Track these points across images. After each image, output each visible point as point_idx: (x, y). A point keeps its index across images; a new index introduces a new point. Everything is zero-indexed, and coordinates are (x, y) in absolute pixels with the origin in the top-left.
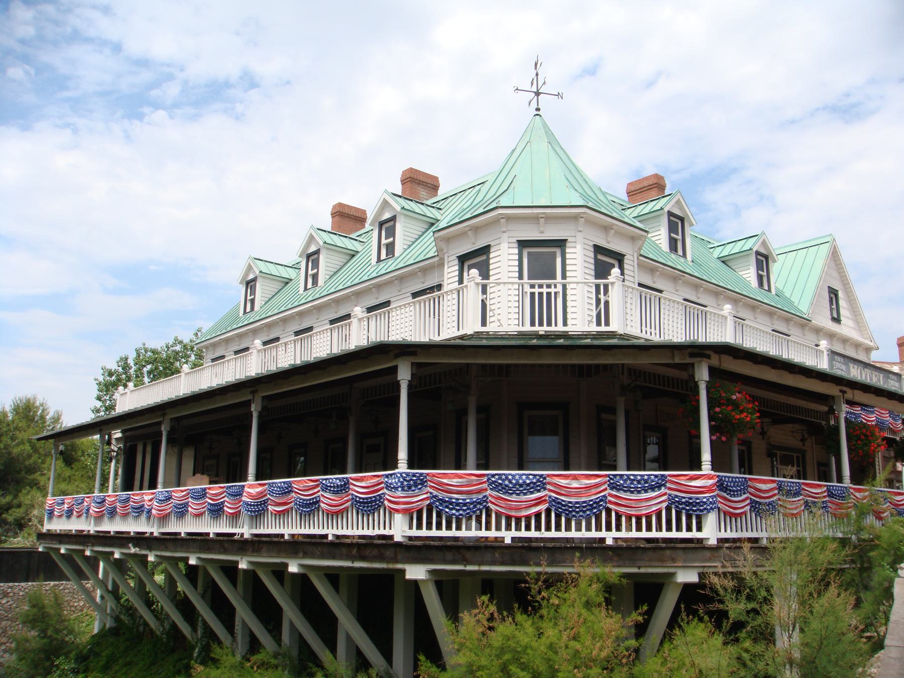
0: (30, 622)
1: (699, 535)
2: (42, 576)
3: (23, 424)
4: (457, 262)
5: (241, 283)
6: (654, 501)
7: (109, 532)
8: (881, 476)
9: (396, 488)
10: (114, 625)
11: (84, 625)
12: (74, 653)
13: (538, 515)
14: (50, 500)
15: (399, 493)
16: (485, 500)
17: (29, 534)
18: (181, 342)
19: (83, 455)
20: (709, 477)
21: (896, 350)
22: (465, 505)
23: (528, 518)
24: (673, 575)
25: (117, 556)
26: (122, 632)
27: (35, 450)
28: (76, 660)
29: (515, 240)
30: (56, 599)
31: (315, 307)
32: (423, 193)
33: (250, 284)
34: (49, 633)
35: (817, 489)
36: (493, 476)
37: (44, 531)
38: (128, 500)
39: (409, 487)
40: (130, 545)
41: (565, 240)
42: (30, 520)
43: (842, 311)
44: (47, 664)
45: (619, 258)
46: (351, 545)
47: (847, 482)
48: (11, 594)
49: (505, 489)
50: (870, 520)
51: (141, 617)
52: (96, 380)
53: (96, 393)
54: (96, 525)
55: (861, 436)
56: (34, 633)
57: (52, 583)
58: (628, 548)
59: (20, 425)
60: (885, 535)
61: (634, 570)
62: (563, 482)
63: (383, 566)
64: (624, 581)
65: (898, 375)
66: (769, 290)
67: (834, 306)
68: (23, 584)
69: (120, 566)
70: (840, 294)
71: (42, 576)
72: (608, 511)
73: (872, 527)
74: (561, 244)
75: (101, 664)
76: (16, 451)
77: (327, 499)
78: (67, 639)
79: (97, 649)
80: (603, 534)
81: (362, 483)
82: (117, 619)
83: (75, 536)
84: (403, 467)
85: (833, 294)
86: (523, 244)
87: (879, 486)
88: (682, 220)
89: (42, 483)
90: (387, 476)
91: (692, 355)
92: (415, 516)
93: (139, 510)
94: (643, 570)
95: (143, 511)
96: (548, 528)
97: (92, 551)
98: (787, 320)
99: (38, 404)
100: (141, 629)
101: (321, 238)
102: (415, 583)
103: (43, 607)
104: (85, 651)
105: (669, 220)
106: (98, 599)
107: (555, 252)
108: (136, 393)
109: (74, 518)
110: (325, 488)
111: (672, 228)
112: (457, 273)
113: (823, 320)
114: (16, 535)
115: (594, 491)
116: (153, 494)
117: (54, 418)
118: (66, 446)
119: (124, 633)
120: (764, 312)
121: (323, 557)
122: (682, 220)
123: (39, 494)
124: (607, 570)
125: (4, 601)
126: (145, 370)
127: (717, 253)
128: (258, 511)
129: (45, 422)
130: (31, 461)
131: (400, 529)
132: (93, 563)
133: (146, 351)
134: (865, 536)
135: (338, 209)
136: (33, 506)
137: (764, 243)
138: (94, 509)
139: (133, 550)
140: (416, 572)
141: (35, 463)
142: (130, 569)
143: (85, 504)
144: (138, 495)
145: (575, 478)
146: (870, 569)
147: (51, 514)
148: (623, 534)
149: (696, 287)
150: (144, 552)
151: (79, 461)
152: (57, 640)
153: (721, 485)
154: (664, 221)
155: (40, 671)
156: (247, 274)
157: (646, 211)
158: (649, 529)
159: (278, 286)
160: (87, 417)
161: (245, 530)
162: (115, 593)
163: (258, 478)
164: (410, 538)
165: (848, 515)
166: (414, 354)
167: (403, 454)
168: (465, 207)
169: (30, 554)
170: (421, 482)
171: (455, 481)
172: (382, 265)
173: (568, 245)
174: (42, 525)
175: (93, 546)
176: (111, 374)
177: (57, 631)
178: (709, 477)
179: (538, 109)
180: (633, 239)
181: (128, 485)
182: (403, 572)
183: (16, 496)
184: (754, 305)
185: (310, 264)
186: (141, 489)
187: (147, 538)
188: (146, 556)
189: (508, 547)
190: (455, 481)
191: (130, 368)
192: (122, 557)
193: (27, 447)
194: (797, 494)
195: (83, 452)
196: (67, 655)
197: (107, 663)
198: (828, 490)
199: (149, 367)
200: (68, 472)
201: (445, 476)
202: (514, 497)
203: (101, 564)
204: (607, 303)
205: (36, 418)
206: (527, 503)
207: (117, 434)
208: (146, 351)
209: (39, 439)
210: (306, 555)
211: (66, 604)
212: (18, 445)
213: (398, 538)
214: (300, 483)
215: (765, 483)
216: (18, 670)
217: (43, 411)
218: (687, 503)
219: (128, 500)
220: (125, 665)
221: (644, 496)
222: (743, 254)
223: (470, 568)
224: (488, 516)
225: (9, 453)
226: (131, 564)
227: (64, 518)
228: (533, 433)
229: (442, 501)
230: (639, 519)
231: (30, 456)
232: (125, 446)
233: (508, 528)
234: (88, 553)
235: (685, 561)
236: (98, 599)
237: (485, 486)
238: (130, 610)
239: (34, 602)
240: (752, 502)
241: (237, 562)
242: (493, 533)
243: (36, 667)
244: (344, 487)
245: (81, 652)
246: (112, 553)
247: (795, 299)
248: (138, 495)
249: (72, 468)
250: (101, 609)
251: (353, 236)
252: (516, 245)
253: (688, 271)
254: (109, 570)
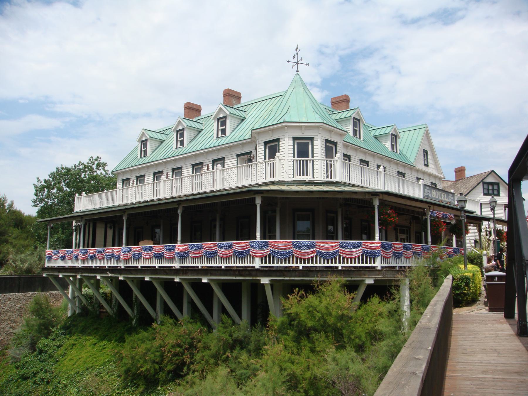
1: (374, 265)
2: (40, 289)
4: (263, 144)
5: (138, 142)
6: (357, 252)
8: (444, 242)
9: (256, 247)
10: (80, 311)
13: (312, 258)
15: (258, 249)
16: (292, 252)
18: (83, 164)
20: (378, 243)
21: (454, 174)
22: (284, 254)
23: (308, 259)
24: (364, 280)
29: (291, 136)
31: (183, 158)
32: (234, 101)
33: (144, 143)
35: (418, 247)
36: (295, 242)
38: (103, 251)
39: (262, 247)
41: (313, 137)
43: (429, 161)
45: (335, 144)
46: (234, 270)
47: (430, 244)
49: (300, 248)
50: (438, 260)
53: (34, 191)
55: (435, 224)
58: (348, 270)
60: (443, 265)
61: (350, 279)
62: (322, 245)
63: (251, 278)
64: (348, 283)
65: (453, 194)
66: (397, 152)
67: (426, 159)
68: (17, 294)
70: (429, 153)
71: (40, 289)
72: (340, 256)
73: (439, 262)
74: (312, 139)
77: (221, 252)
80: (299, 265)
81: (239, 245)
84: (258, 239)
85: (425, 152)
86: (294, 139)
87: (442, 245)
88: (359, 121)
90: (251, 242)
92: (263, 258)
94: (353, 279)
96: (270, 263)
98: (404, 166)
101: (185, 123)
102: (263, 285)
105: (354, 121)
107: (308, 143)
110: (220, 247)
111: (355, 125)
112: (263, 149)
113: (420, 166)
115: (334, 248)
120: (394, 163)
121: (221, 275)
122: (359, 121)
124: (341, 279)
125: (8, 303)
127: (373, 133)
128: (184, 257)
131: (258, 264)
133: (63, 168)
134: (436, 266)
135: (188, 105)
137: (395, 130)
140: (265, 281)
145: (327, 243)
146: (437, 279)
148: (345, 265)
149: (365, 153)
153: (382, 246)
154: (351, 122)
156: (141, 137)
157: (343, 116)
158: (355, 263)
159: (158, 143)
161: (177, 265)
163: (182, 242)
164: (262, 267)
165: (430, 258)
167: (258, 234)
168: (266, 118)
170: (266, 245)
171: (279, 244)
172: (220, 140)
173: (315, 139)
175: (82, 273)
178: (378, 243)
179: (297, 71)
180: (341, 135)
182: (260, 280)
184: (390, 160)
185: (179, 135)
187: (119, 269)
188: (119, 277)
189: (301, 270)
190: (279, 244)
194: (410, 249)
198: (422, 247)
201: (276, 242)
202: (303, 251)
206: (308, 253)
210: (212, 275)
213: (257, 267)
214: (206, 245)
215: (399, 245)
218: (370, 253)
219: (103, 251)
221: (353, 250)
222: (385, 135)
223: (286, 278)
224: (340, 258)
228: (299, 220)
229: (275, 252)
230: (351, 259)
233: (301, 263)
235: (369, 275)
237: (292, 246)
240: (394, 252)
241: (174, 279)
242: (295, 265)
244: (231, 246)
247: (408, 155)
251: (194, 120)
252: (292, 139)
253: (362, 146)
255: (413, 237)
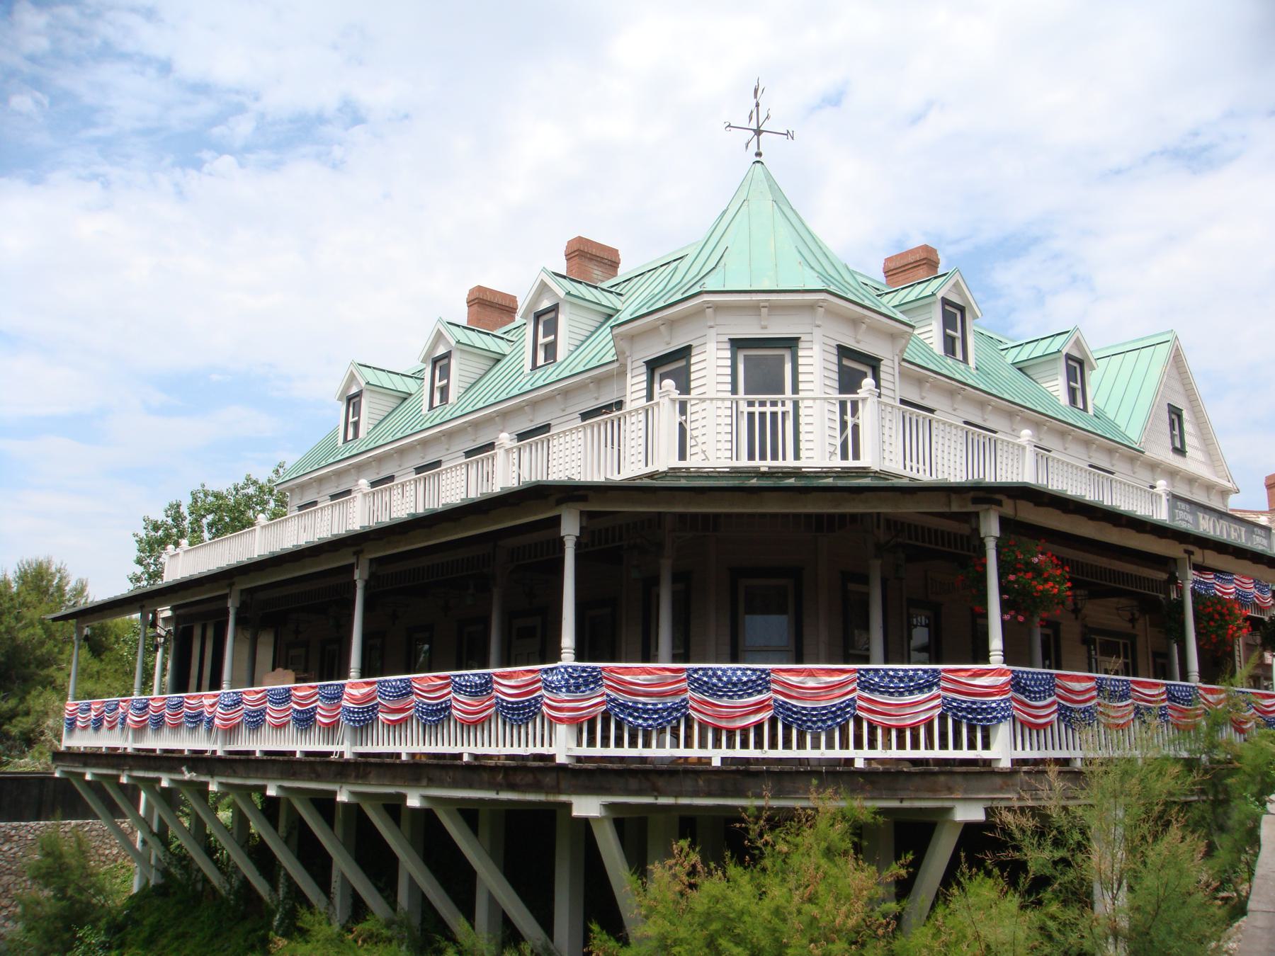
0: (43, 877)
1: (986, 755)
2: (59, 812)
3: (33, 598)
4: (644, 369)
5: (340, 399)
6: (923, 707)
7: (154, 751)
8: (1243, 671)
9: (559, 689)
10: (161, 881)
11: (119, 881)
12: (104, 920)
13: (759, 727)
14: (70, 705)
15: (563, 695)
16: (685, 704)
17: (41, 753)
18: (255, 483)
19: (117, 642)
20: (1000, 673)
21: (1264, 493)
22: (656, 711)
23: (745, 730)
24: (949, 810)
25: (165, 784)
26: (171, 891)
27: (50, 635)
28: (108, 931)
29: (726, 338)
30: (80, 844)
31: (444, 433)
32: (597, 272)
33: (353, 401)
34: (70, 892)
35: (1153, 690)
36: (696, 671)
37: (63, 749)
38: (180, 705)
39: (578, 687)
40: (184, 769)
41: (798, 339)
42: (42, 733)
43: (1187, 439)
44: (67, 936)
45: (874, 364)
46: (495, 769)
47: (1194, 679)
48: (16, 838)
49: (713, 690)
50: (1227, 733)
51: (199, 870)
52: (136, 535)
53: (135, 554)
54: (135, 740)
55: (1214, 614)
56: (48, 893)
57: (73, 822)
58: (886, 773)
59: (28, 599)
60: (1249, 754)
61: (894, 804)
62: (794, 680)
63: (541, 797)
64: (880, 819)
65: (1267, 529)
66: (1085, 409)
67: (1176, 432)
68: (32, 824)
69: (169, 798)
70: (1185, 415)
71: (59, 812)
72: (858, 721)
73: (1230, 743)
74: (791, 344)
75: (142, 936)
76: (22, 636)
77: (461, 704)
78: (94, 901)
79: (137, 915)
81: (510, 681)
82: (165, 873)
83: (106, 756)
84: (568, 658)
85: (1175, 414)
86: (737, 344)
87: (1240, 686)
88: (962, 310)
89: (59, 682)
90: (546, 671)
91: (976, 501)
92: (586, 727)
93: (196, 719)
94: (906, 804)
95: (201, 721)
96: (773, 745)
97: (129, 776)
98: (1110, 452)
99: (53, 569)
100: (199, 887)
101: (453, 335)
102: (586, 822)
103: (61, 856)
104: (120, 918)
105: (944, 311)
106: (138, 845)
107: (783, 356)
108: (192, 554)
109: (104, 730)
110: (459, 688)
111: (948, 321)
112: (644, 385)
113: (1161, 452)
114: (22, 755)
115: (837, 692)
116: (215, 696)
117: (75, 590)
118: (93, 629)
119: (175, 893)
120: (1078, 440)
121: (455, 785)
122: (962, 310)
123: (55, 697)
124: (856, 804)
125: (6, 848)
126: (205, 521)
127: (1011, 356)
128: (364, 721)
129: (63, 595)
130: (44, 650)
131: (564, 746)
132: (131, 793)
133: (206, 495)
134: (1220, 755)
135: (476, 295)
136: (47, 714)
137: (1078, 343)
138: (132, 718)
139: (187, 776)
140: (587, 807)
141: (50, 653)
142: (183, 803)
143: (121, 710)
144: (194, 697)
145: (811, 673)
146: (1226, 802)
147: (72, 724)
148: (879, 753)
149: (982, 405)
150: (203, 779)
151: (111, 649)
152: (80, 902)
153: (1017, 685)
154: (937, 312)
155: (56, 946)
156: (348, 387)
157: (911, 297)
158: (915, 745)
159: (392, 403)
160: (123, 588)
161: (346, 748)
162: (162, 836)
163: (363, 674)
164: (579, 759)
165: (1196, 727)
166: (584, 499)
167: (568, 640)
168: (656, 291)
169: (43, 781)
170: (593, 680)
171: (641, 679)
172: (539, 373)
173: (801, 345)
174: (60, 741)
175: (131, 769)
176: (156, 527)
177: (81, 890)
178: (1000, 673)
179: (759, 154)
180: (893, 337)
181: (180, 684)
182: (568, 806)
183: (22, 700)
184: (1064, 430)
185: (437, 372)
186: (199, 689)
187: (207, 759)
188: (207, 784)
189: (717, 771)
190: (641, 679)
191: (184, 519)
192: (173, 785)
193: (39, 631)
194: (1124, 696)
195: (117, 638)
196: (94, 924)
197: (151, 934)
198: (1168, 692)
199: (210, 517)
200: (95, 666)
201: (628, 671)
202: (725, 701)
203: (143, 796)
204: (856, 428)
205: (51, 590)
206: (743, 710)
207: (165, 612)
208: (206, 495)
209: (55, 620)
210: (432, 783)
211: (93, 851)
212: (26, 627)
213: (561, 759)
214: (423, 680)
215: (1079, 682)
216: (25, 944)
217: (61, 579)
218: (969, 710)
219: (180, 705)
220: (177, 938)
221: (908, 699)
222: (1048, 358)
223: (663, 801)
224: (689, 727)
225: (13, 639)
226: (185, 795)
227: (90, 730)
229: (624, 706)
230: (901, 731)
231: (42, 643)
232: (176, 629)
233: (717, 744)
234: (124, 780)
235: (966, 791)
236: (138, 845)
237: (684, 685)
238: (183, 860)
239: (48, 849)
240: (1061, 707)
241: (334, 793)
242: (695, 752)
243: (51, 940)
244: (485, 687)
245: (114, 919)
246: (159, 780)
247: (1121, 422)
248: (194, 697)
249: (102, 660)
250: (142, 858)
251: (498, 332)
252: (728, 346)
253: (970, 382)
254: (154, 803)
255: (1144, 660)
